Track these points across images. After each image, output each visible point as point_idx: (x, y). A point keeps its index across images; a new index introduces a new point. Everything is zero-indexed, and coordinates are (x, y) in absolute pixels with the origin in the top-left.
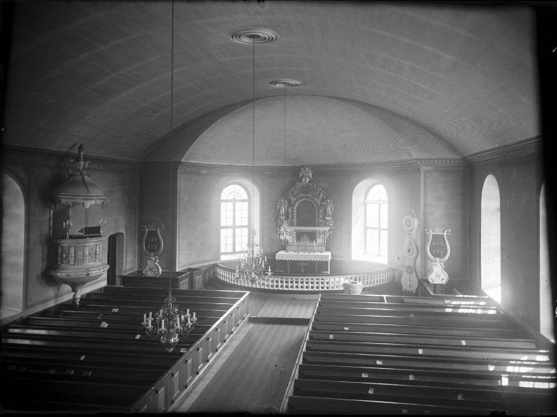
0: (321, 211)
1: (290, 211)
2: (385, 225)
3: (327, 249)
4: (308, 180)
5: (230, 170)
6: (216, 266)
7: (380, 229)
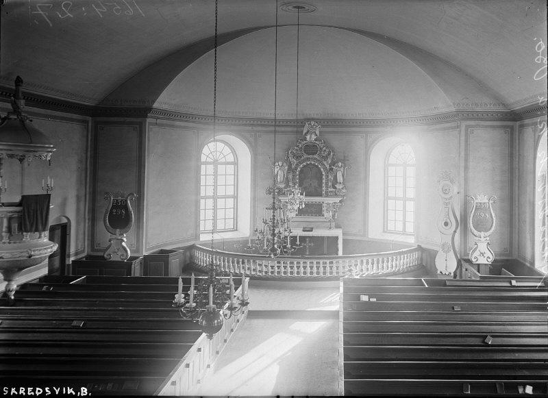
0: (330, 177)
1: (290, 176)
2: (411, 193)
3: (338, 227)
4: (314, 137)
5: (214, 120)
6: (193, 247)
7: (405, 199)
